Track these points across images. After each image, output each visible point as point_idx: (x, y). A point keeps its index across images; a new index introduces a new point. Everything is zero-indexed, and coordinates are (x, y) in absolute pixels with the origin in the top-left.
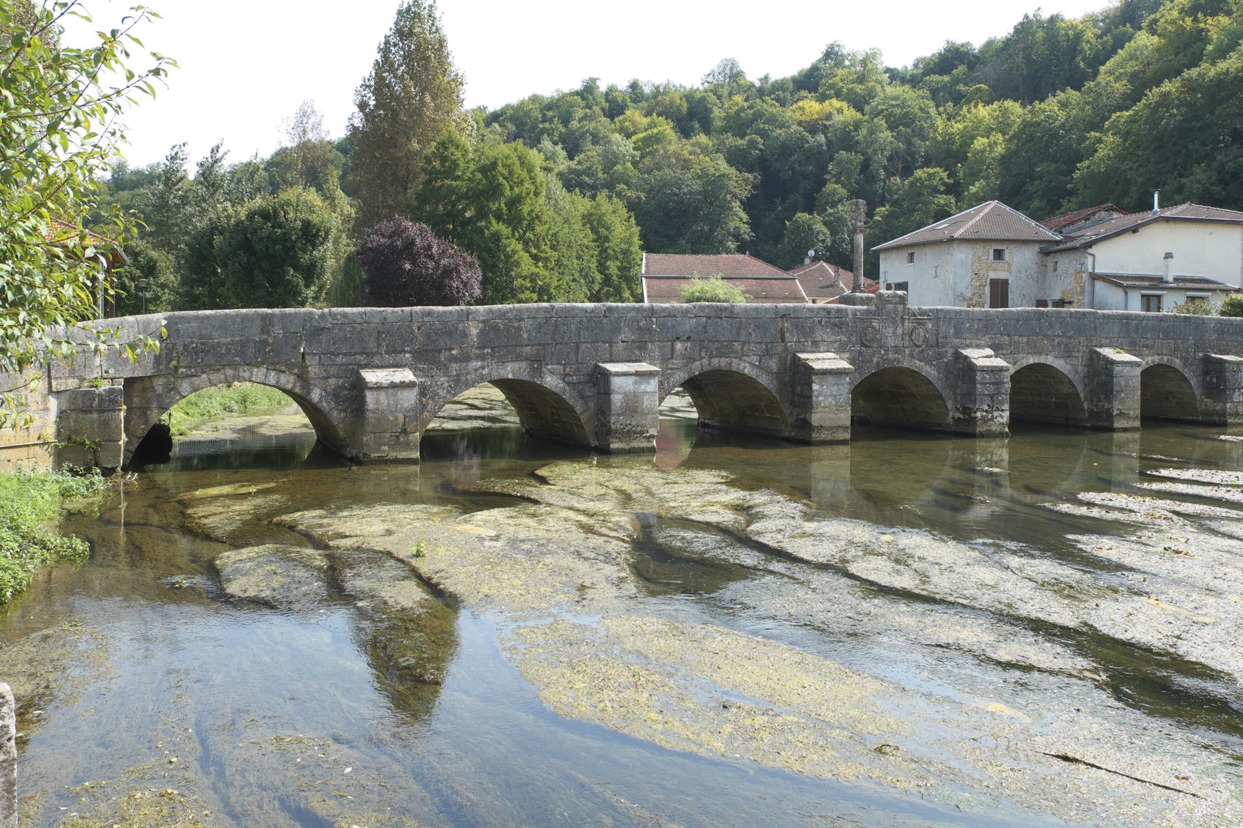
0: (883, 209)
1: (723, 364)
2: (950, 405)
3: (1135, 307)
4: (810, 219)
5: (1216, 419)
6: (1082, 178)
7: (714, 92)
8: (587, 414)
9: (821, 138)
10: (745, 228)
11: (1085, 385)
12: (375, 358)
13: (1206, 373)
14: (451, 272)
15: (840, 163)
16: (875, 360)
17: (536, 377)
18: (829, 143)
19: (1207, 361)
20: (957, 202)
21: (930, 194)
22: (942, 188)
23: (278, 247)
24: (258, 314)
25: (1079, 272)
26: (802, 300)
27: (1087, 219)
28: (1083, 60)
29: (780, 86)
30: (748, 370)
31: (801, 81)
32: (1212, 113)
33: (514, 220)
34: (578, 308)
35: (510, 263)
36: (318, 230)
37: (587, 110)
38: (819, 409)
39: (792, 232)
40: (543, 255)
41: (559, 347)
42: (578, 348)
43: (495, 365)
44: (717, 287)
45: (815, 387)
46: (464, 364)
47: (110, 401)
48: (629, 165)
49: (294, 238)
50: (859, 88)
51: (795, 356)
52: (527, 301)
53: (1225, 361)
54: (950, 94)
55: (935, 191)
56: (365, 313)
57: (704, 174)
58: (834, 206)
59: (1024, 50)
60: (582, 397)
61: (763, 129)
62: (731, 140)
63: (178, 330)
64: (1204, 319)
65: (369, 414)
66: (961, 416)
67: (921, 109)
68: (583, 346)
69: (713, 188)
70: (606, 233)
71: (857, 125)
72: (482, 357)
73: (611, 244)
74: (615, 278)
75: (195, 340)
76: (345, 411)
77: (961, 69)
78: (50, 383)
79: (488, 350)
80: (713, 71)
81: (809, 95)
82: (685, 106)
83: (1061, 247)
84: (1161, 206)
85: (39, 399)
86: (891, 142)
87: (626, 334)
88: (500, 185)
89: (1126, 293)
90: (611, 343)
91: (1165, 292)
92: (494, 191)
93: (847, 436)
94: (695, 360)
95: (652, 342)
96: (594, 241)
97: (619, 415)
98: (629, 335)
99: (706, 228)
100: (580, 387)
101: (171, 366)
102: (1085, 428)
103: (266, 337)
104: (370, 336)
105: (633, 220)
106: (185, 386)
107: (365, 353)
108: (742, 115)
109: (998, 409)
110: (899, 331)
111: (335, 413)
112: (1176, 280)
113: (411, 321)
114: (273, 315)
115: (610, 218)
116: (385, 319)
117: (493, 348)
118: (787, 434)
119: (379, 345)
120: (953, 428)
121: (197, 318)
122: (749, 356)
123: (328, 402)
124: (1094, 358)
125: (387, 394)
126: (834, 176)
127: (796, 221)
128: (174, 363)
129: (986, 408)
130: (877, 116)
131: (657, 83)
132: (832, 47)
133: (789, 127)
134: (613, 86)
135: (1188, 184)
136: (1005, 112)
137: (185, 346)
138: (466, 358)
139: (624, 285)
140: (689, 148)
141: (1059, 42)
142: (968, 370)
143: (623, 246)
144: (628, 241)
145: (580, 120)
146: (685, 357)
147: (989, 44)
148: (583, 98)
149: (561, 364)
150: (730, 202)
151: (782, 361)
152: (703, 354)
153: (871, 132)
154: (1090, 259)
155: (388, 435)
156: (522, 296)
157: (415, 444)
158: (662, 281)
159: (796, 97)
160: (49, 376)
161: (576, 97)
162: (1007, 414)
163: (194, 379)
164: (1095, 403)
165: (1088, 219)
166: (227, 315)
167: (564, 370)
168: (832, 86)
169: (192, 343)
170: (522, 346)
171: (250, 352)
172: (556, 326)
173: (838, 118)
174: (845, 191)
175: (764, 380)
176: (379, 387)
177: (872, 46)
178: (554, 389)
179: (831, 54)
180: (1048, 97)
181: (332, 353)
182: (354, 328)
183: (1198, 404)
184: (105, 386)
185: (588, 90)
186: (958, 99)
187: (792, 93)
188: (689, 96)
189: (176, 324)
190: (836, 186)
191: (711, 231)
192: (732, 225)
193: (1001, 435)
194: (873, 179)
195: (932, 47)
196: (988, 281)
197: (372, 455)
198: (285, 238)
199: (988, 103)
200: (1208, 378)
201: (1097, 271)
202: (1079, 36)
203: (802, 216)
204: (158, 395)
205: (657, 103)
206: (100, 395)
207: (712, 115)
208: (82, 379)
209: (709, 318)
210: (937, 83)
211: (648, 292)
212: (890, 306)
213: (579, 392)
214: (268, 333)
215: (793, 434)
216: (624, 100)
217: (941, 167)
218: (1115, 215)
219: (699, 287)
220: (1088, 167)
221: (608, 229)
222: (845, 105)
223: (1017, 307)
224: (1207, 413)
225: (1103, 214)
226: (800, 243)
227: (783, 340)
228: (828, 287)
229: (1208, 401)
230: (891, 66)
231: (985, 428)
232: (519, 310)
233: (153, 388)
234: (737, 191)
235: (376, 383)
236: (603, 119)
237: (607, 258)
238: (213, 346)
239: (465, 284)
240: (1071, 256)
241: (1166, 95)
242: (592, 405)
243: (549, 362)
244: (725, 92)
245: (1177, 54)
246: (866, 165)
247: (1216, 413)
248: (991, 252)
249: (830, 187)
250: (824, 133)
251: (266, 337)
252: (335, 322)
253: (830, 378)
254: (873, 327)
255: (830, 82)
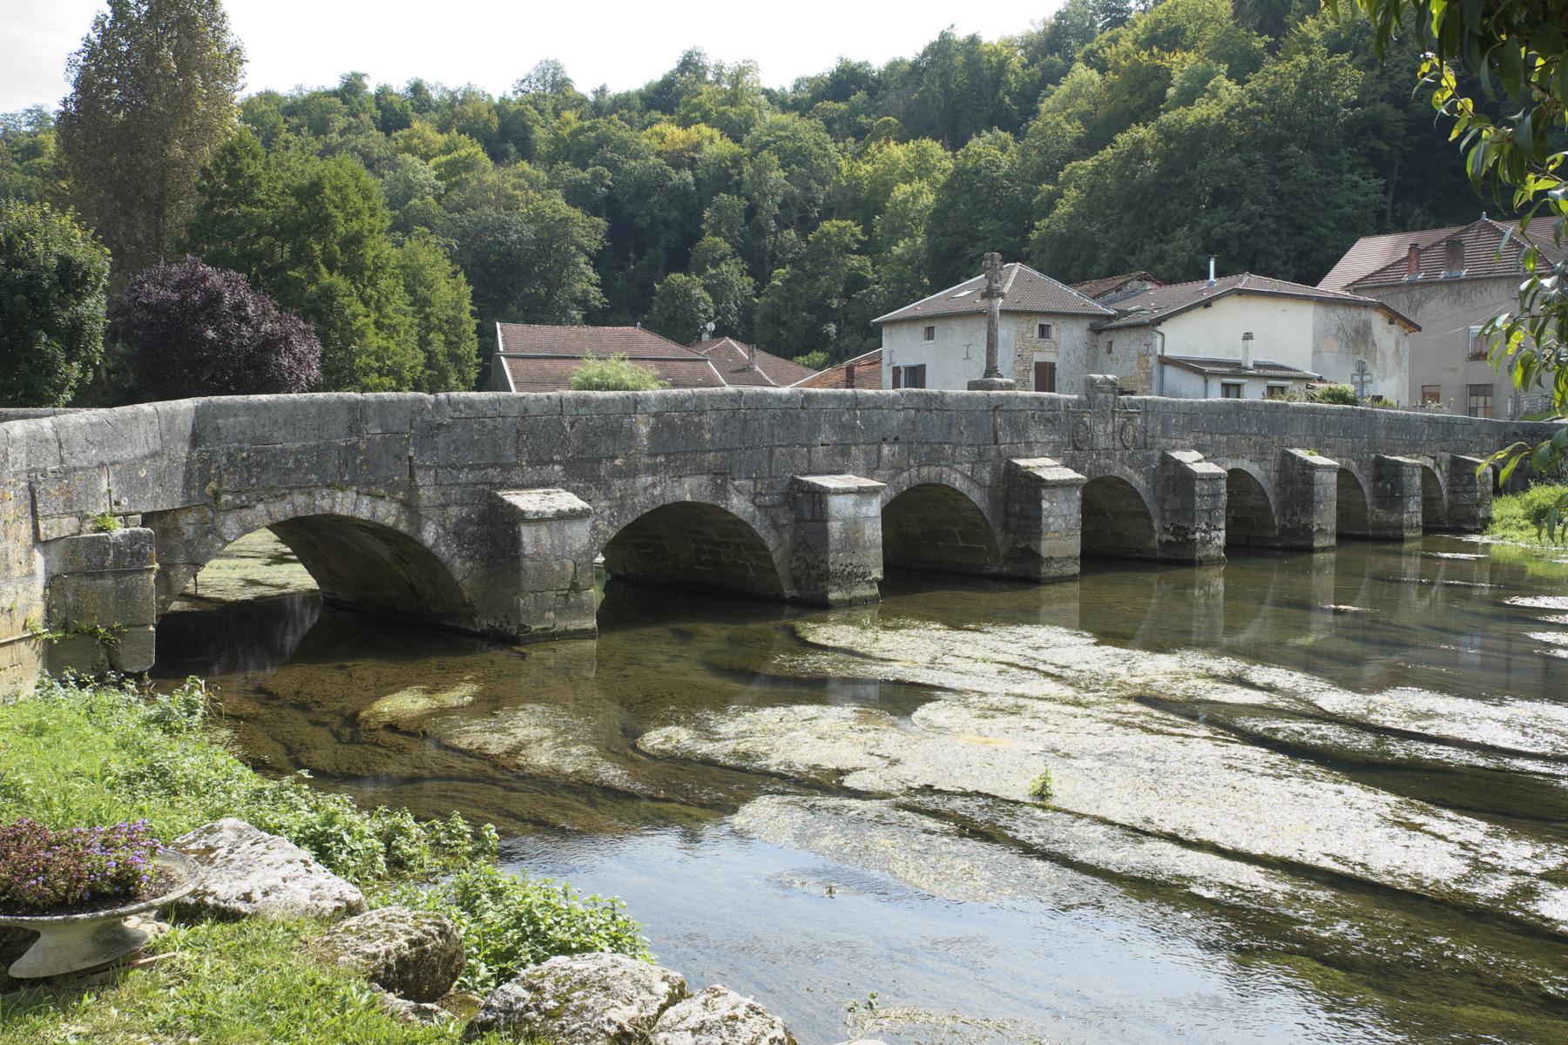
0: (783, 271)
1: (933, 475)
2: (1156, 524)
3: (1216, 397)
4: (688, 282)
5: (1391, 533)
6: (1041, 241)
7: (534, 104)
8: (781, 550)
9: (688, 176)
10: (595, 292)
11: (1277, 496)
12: (513, 473)
13: (1378, 478)
14: (276, 344)
15: (719, 209)
16: (1087, 466)
17: (719, 498)
18: (698, 181)
19: (1380, 463)
20: (874, 265)
21: (839, 254)
22: (855, 247)
23: (20, 298)
24: (342, 401)
25: (1143, 356)
26: (712, 383)
27: (1118, 290)
28: (1008, 93)
29: (622, 104)
30: (959, 483)
31: (651, 99)
32: (1194, 166)
33: (354, 271)
34: (771, 395)
35: (351, 334)
36: (86, 274)
37: (351, 119)
38: (1050, 535)
39: (663, 298)
40: (387, 321)
41: (749, 452)
42: (771, 454)
43: (669, 482)
44: (622, 370)
45: (1045, 505)
46: (631, 481)
47: (133, 555)
48: (430, 199)
49: (46, 284)
50: (732, 112)
51: (1009, 463)
52: (375, 388)
53: (1402, 464)
54: (849, 126)
55: (848, 250)
56: (498, 400)
57: (537, 217)
58: (716, 264)
59: (940, 75)
60: (776, 526)
61: (611, 159)
62: (568, 172)
63: (218, 429)
64: (1375, 413)
65: (527, 563)
66: (1172, 539)
67: (817, 144)
68: (777, 451)
69: (551, 235)
70: (427, 293)
71: (736, 161)
72: (652, 470)
73: (434, 310)
74: (440, 357)
75: (247, 446)
76: (472, 558)
77: (860, 96)
78: (36, 528)
79: (661, 459)
80: (529, 76)
81: (664, 118)
82: (495, 122)
83: (1115, 323)
84: (1218, 275)
85: (22, 555)
86: (784, 185)
87: (826, 435)
88: (329, 216)
89: (1206, 381)
90: (810, 447)
91: (1245, 381)
92: (320, 224)
93: (1076, 569)
94: (902, 470)
95: (856, 444)
96: (411, 305)
97: (838, 552)
98: (830, 434)
99: (542, 291)
100: (774, 511)
101: (207, 490)
102: (1273, 548)
103: (355, 439)
104: (505, 438)
105: (461, 276)
106: (230, 524)
107: (500, 465)
108: (581, 138)
109: (1215, 529)
110: (1110, 428)
111: (458, 562)
112: (1257, 366)
113: (561, 414)
114: (366, 403)
115: (429, 274)
116: (526, 410)
117: (667, 455)
118: (995, 570)
119: (518, 452)
120: (1159, 554)
121: (248, 407)
122: (961, 463)
123: (447, 545)
124: (1288, 460)
125: (550, 530)
126: (712, 226)
127: (669, 283)
128: (213, 485)
129: (1204, 527)
130: (761, 149)
131: (451, 87)
132: (690, 55)
133: (647, 159)
134: (385, 87)
135: (1171, 252)
136: (922, 155)
137: (230, 455)
138: (631, 472)
139: (450, 367)
140: (514, 180)
141: (981, 70)
142: (1185, 476)
143: (451, 313)
144: (457, 306)
145: (342, 133)
146: (893, 467)
147: (893, 66)
148: (345, 102)
149: (751, 478)
150: (574, 256)
151: (995, 469)
152: (912, 462)
153: (759, 171)
154: (1159, 339)
155: (553, 594)
156: (365, 380)
157: (590, 607)
158: (530, 362)
159: (647, 117)
160: (34, 513)
161: (333, 99)
162: (1223, 534)
163: (245, 512)
164: (1288, 517)
165: (1120, 290)
166: (295, 402)
167: (755, 488)
168: (698, 107)
169: (242, 450)
170: (703, 452)
171: (332, 464)
172: (746, 421)
173: (709, 150)
174: (727, 245)
175: (976, 496)
176: (540, 519)
177: (746, 58)
178: (741, 516)
179: (690, 64)
180: (971, 138)
181: (454, 466)
182: (484, 425)
183: (1369, 514)
184: (118, 531)
185: (351, 88)
186: (861, 134)
187: (642, 113)
188: (501, 108)
189: (215, 417)
190: (717, 239)
191: (549, 295)
192: (579, 288)
193: (1219, 561)
194: (760, 232)
195: (822, 66)
196: (1033, 365)
197: (534, 628)
198: (31, 284)
199: (902, 140)
200: (1380, 484)
201: (1166, 354)
202: (1002, 64)
203: (677, 278)
204: (188, 541)
205: (455, 116)
206: (116, 545)
207: (533, 137)
208: (83, 518)
209: (918, 410)
210: (832, 111)
211: (513, 376)
212: (1101, 395)
213: (772, 519)
214: (358, 433)
215: (1005, 569)
216: (403, 108)
217: (853, 220)
218: (1149, 286)
219: (597, 371)
220: (1048, 227)
221: (429, 288)
222: (716, 133)
223: (1063, 395)
224: (1379, 526)
225: (1136, 284)
226: (675, 312)
227: (996, 443)
228: (739, 371)
229: (1381, 512)
230: (767, 87)
231: (1204, 553)
232: (700, 397)
233: (179, 529)
234: (585, 241)
235: (537, 513)
236: (375, 132)
237: (429, 329)
238: (274, 456)
239: (300, 362)
240: (1133, 335)
241: (1139, 143)
242: (787, 537)
243: (736, 475)
244: (549, 106)
245: (1131, 93)
246: (751, 212)
247: (1389, 526)
248: (1037, 328)
249: (708, 240)
250: (691, 168)
251: (355, 439)
252: (457, 415)
253: (1060, 493)
254: (1085, 424)
255: (695, 101)
